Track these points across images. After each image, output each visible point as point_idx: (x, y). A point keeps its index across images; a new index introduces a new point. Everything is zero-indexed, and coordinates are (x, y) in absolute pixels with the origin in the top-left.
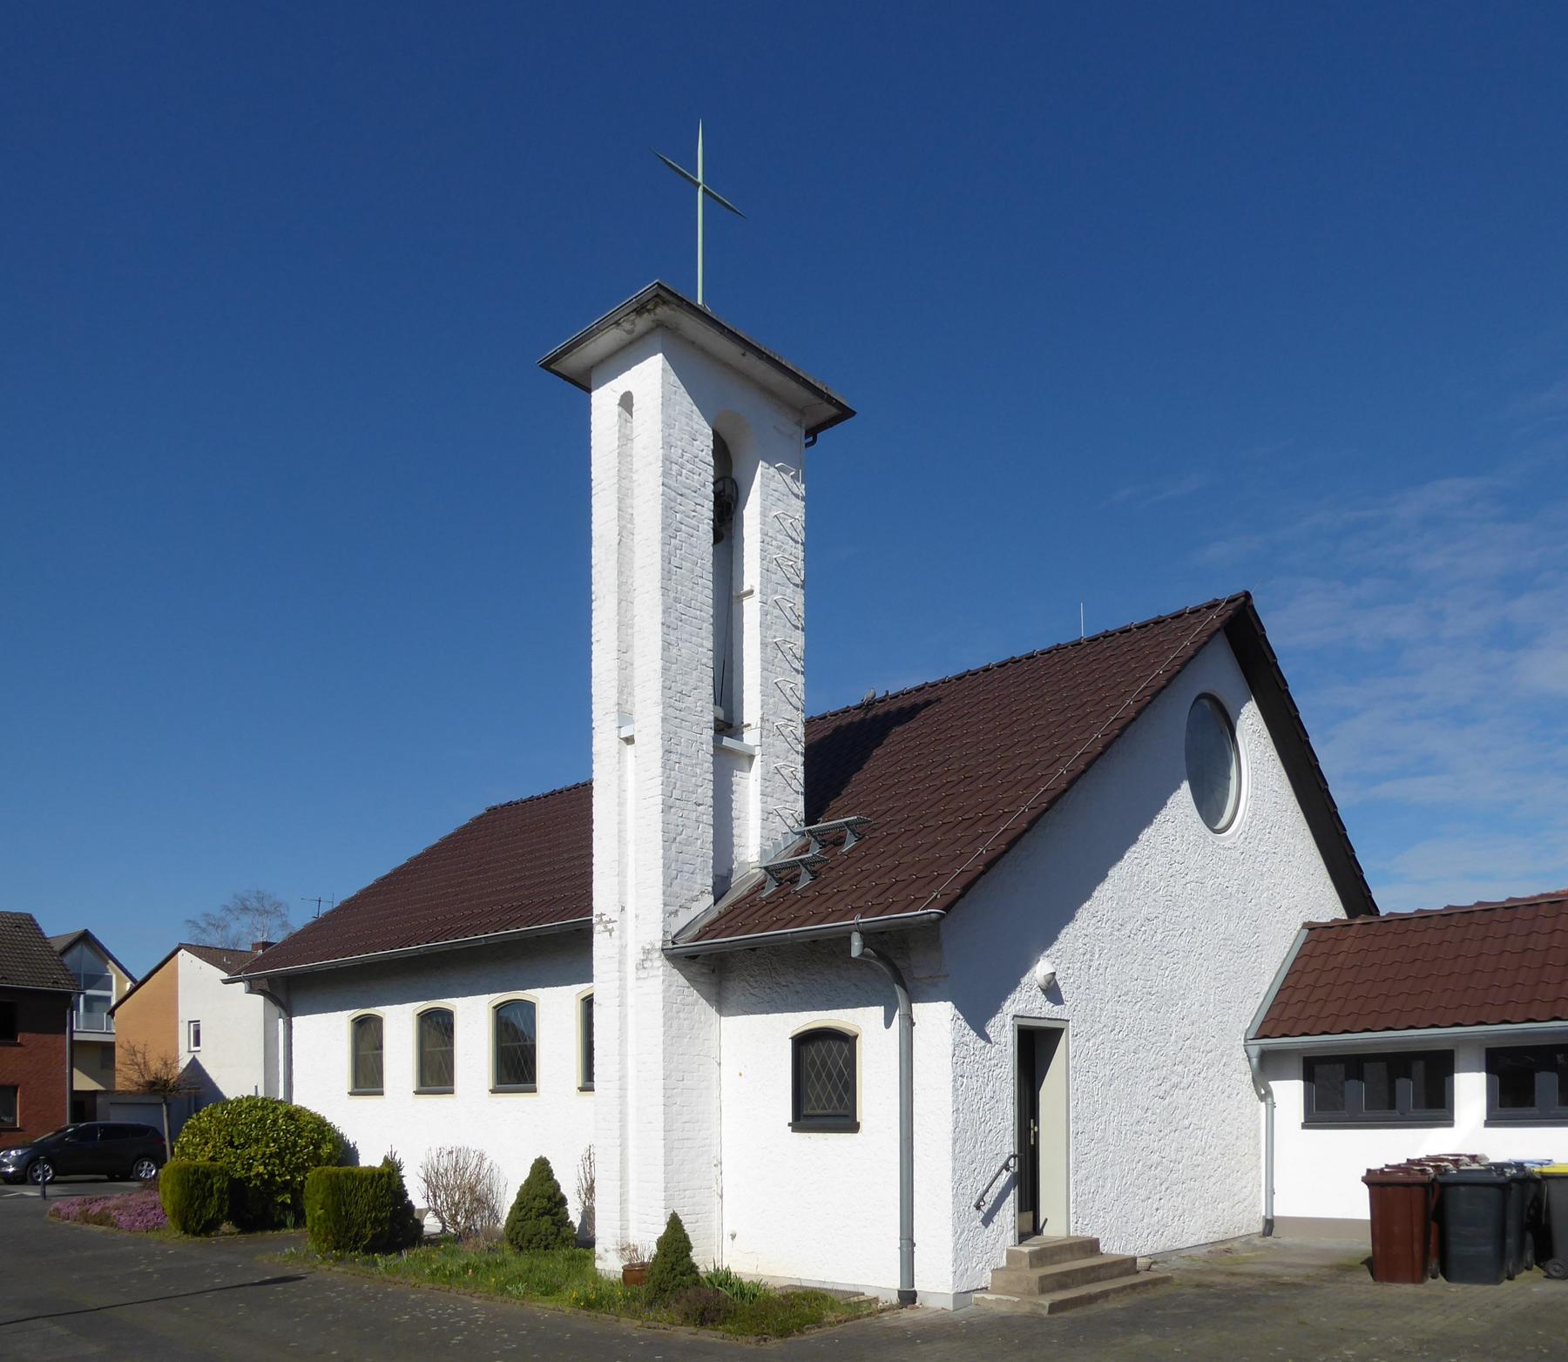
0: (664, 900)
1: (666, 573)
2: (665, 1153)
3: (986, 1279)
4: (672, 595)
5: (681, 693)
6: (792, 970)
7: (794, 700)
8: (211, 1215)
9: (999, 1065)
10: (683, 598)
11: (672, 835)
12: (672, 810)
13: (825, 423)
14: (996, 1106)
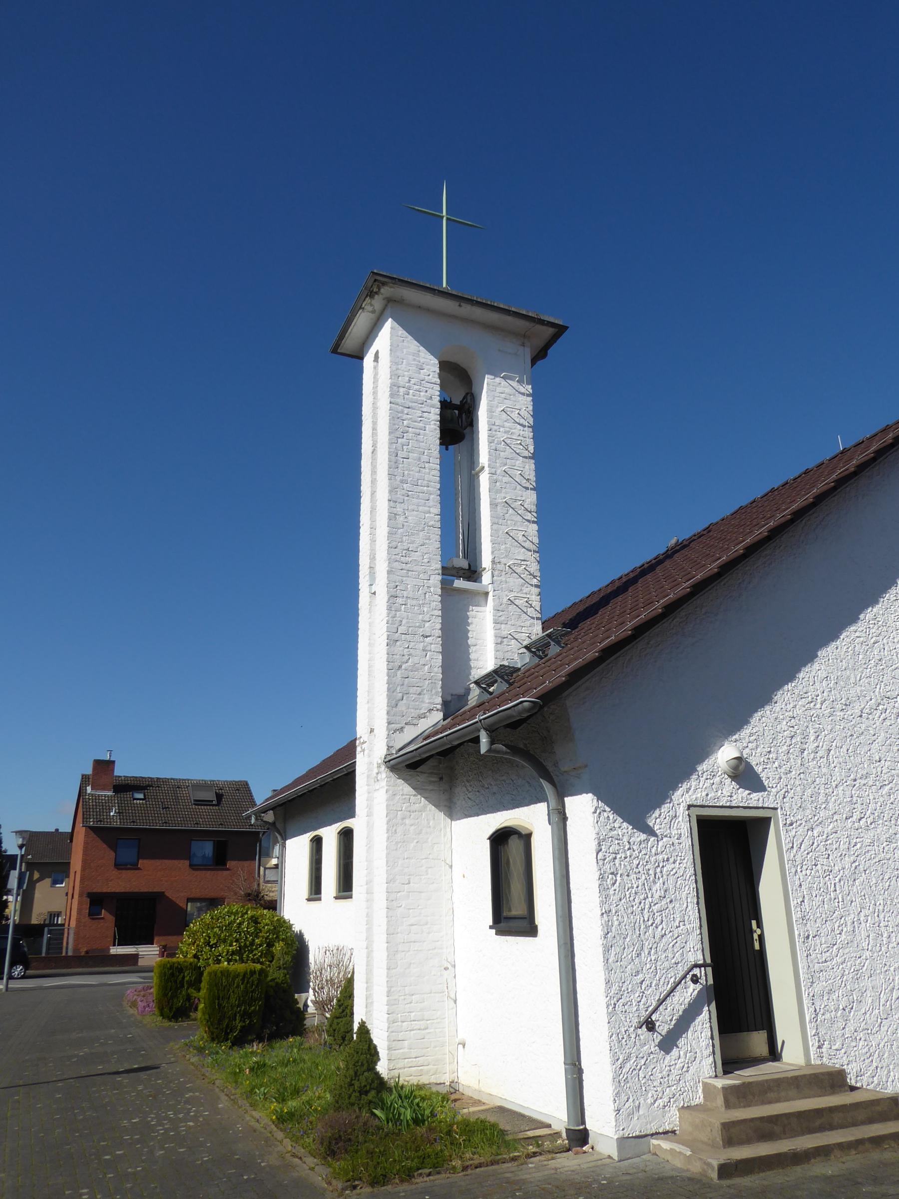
0: (388, 719)
1: (392, 463)
2: (388, 956)
3: (672, 1119)
4: (398, 478)
5: (408, 550)
6: (490, 772)
7: (528, 544)
8: (180, 1004)
9: (671, 860)
10: (409, 479)
11: (397, 664)
12: (398, 643)
13: (550, 341)
14: (671, 906)
